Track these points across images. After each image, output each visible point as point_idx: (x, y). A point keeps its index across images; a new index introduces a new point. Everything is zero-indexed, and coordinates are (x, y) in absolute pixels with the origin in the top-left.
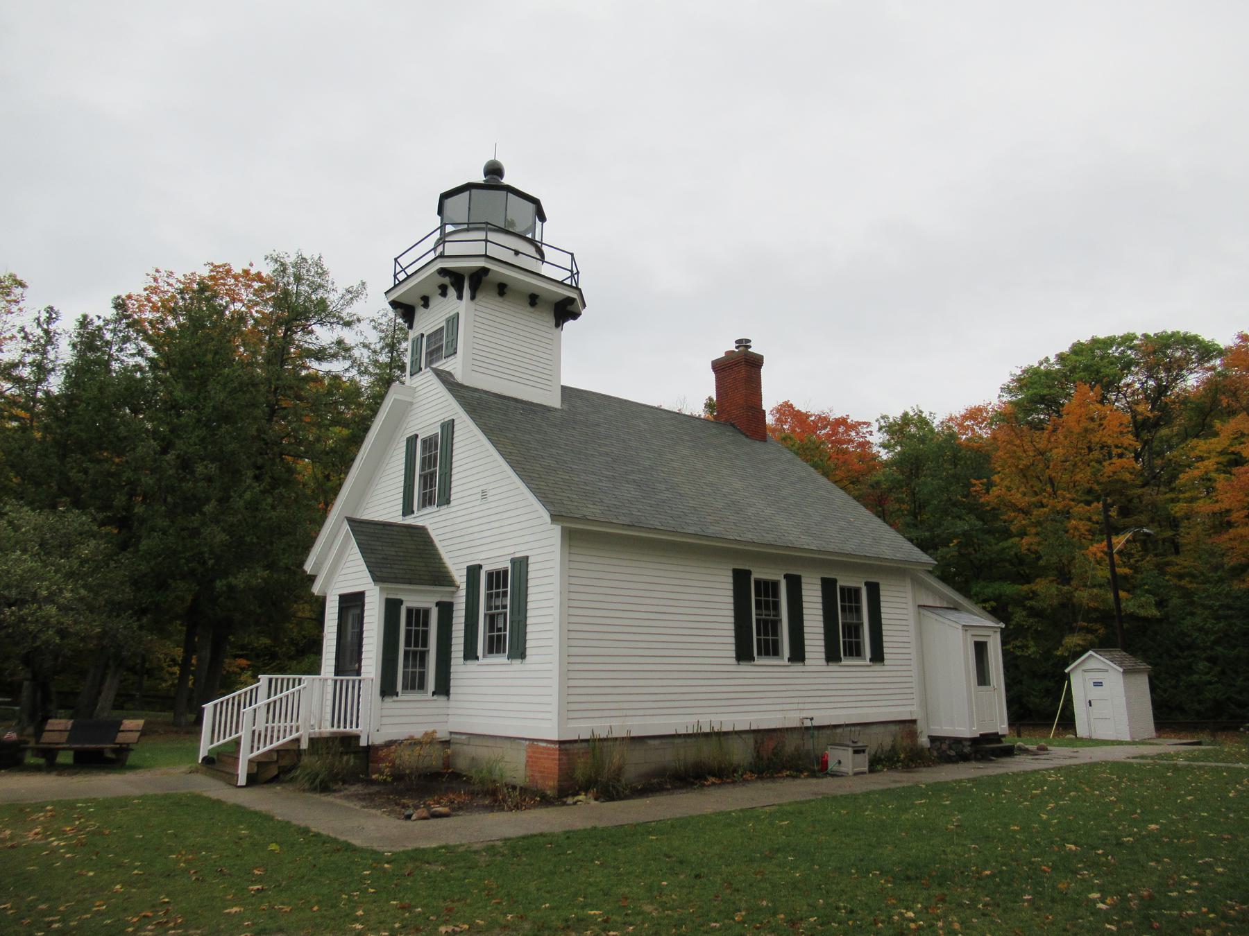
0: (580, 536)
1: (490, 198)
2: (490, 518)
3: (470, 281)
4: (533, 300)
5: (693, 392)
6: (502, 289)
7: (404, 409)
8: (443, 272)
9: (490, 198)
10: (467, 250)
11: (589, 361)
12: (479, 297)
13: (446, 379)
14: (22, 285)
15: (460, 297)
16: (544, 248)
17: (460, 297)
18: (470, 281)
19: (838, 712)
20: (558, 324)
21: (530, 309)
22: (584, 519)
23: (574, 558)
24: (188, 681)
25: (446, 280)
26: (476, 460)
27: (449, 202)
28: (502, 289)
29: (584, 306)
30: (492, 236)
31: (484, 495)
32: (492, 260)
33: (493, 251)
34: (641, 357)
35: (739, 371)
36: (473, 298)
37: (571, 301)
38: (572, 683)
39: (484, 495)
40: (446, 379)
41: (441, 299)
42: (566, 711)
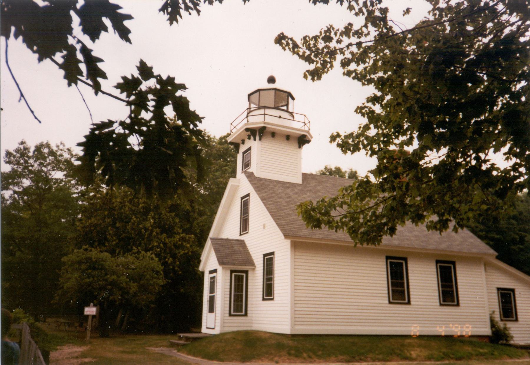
0: (298, 245)
4: (288, 137)
6: (273, 134)
7: (236, 189)
8: (247, 130)
10: (257, 120)
12: (262, 140)
14: (293, 99)
15: (255, 140)
16: (294, 114)
17: (255, 140)
18: (257, 133)
19: (397, 329)
20: (300, 147)
21: (287, 141)
22: (300, 237)
23: (297, 254)
24: (522, 88)
25: (249, 133)
27: (252, 97)
28: (273, 134)
29: (312, 137)
30: (268, 111)
31: (264, 226)
33: (268, 119)
36: (260, 139)
37: (304, 136)
38: (297, 309)
39: (264, 226)
41: (248, 140)
42: (294, 322)
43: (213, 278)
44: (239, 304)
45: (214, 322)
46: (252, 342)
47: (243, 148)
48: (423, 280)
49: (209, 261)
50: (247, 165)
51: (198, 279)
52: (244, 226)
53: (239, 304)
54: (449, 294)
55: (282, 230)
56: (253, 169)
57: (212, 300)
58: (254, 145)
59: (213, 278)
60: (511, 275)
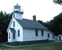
0: (24, 28)
1: (17, 7)
2: (18, 27)
3: (16, 12)
5: (32, 19)
7: (12, 21)
9: (17, 7)
10: (16, 10)
11: (24, 16)
13: (15, 18)
18: (16, 12)
26: (17, 23)
32: (18, 10)
34: (28, 16)
35: (34, 17)
40: (15, 18)
42: (24, 39)
43: (10, 34)
44: (14, 37)
45: (10, 40)
46: (18, 43)
47: (13, 14)
48: (40, 33)
49: (9, 31)
50: (14, 17)
51: (7, 34)
52: (14, 26)
53: (14, 37)
54: (42, 35)
55: (22, 27)
56: (15, 17)
57: (10, 37)
58: (15, 14)
59: (10, 34)
60: (11, 23)
